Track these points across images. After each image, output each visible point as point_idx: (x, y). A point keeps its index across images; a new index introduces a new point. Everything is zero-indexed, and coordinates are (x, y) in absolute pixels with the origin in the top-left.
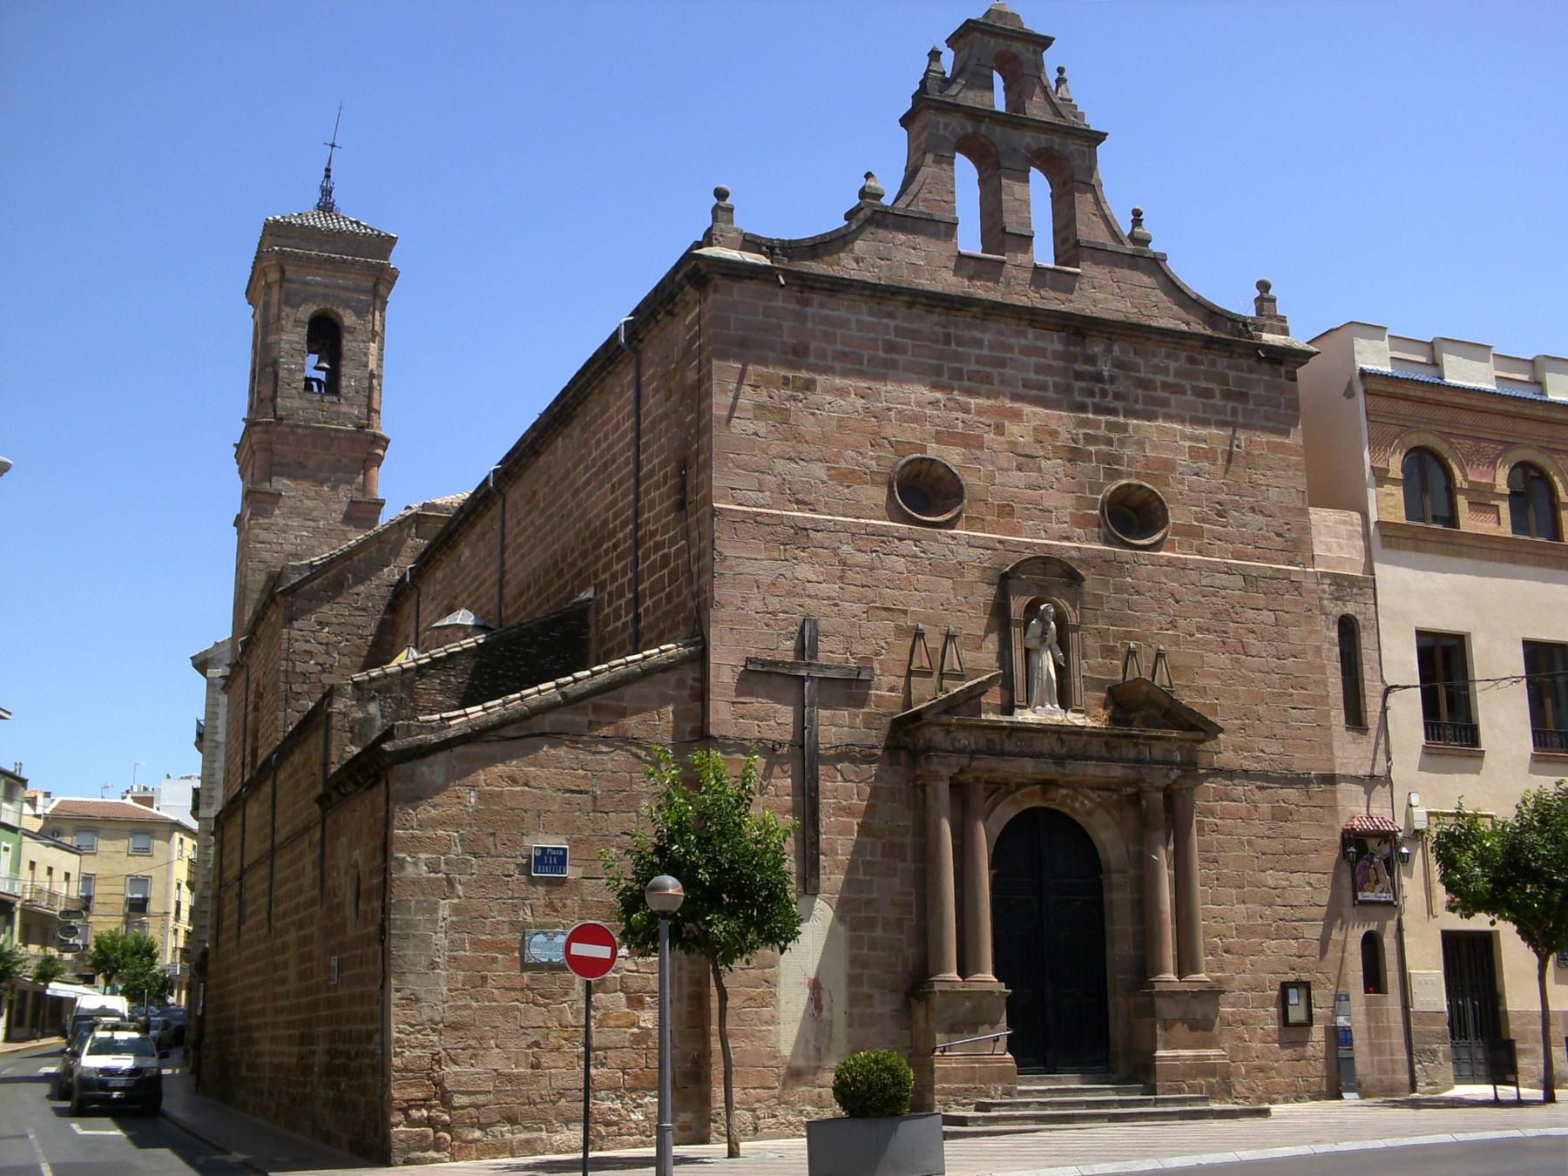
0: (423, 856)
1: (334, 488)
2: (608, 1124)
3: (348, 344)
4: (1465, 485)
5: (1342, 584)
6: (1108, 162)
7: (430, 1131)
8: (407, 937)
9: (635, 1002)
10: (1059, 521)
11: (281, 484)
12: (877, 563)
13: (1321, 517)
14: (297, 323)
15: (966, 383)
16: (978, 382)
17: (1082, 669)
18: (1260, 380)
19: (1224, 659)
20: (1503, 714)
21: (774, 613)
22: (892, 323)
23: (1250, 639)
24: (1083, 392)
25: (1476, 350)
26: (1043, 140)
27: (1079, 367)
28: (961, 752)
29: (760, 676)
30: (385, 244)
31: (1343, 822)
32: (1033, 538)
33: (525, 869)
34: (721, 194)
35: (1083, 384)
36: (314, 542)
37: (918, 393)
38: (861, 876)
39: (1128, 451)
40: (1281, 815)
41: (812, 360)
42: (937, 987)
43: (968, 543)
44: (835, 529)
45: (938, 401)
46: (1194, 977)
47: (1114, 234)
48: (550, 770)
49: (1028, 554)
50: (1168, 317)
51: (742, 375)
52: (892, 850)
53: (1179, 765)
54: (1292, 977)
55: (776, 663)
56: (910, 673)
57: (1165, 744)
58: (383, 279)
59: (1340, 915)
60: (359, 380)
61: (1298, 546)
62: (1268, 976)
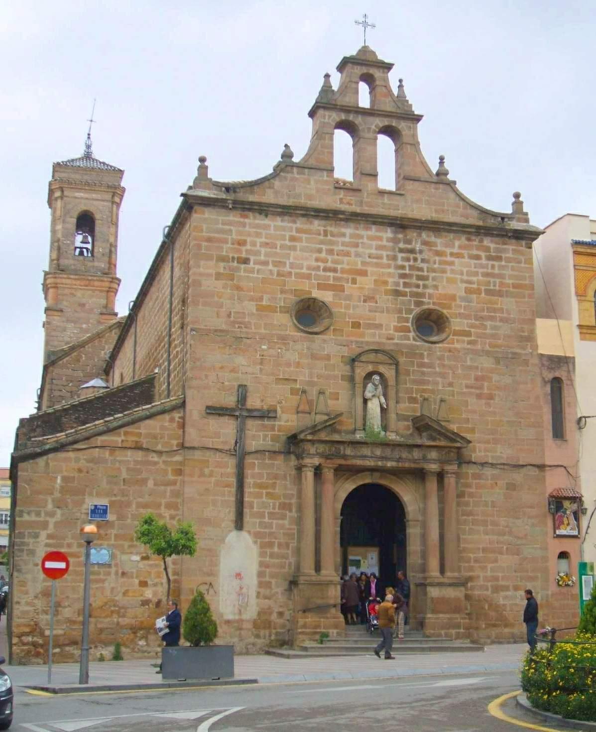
3: (98, 228)
15: (336, 257)
27: (402, 245)
32: (371, 337)
35: (403, 255)
38: (266, 520)
43: (332, 346)
47: (429, 171)
58: (116, 193)
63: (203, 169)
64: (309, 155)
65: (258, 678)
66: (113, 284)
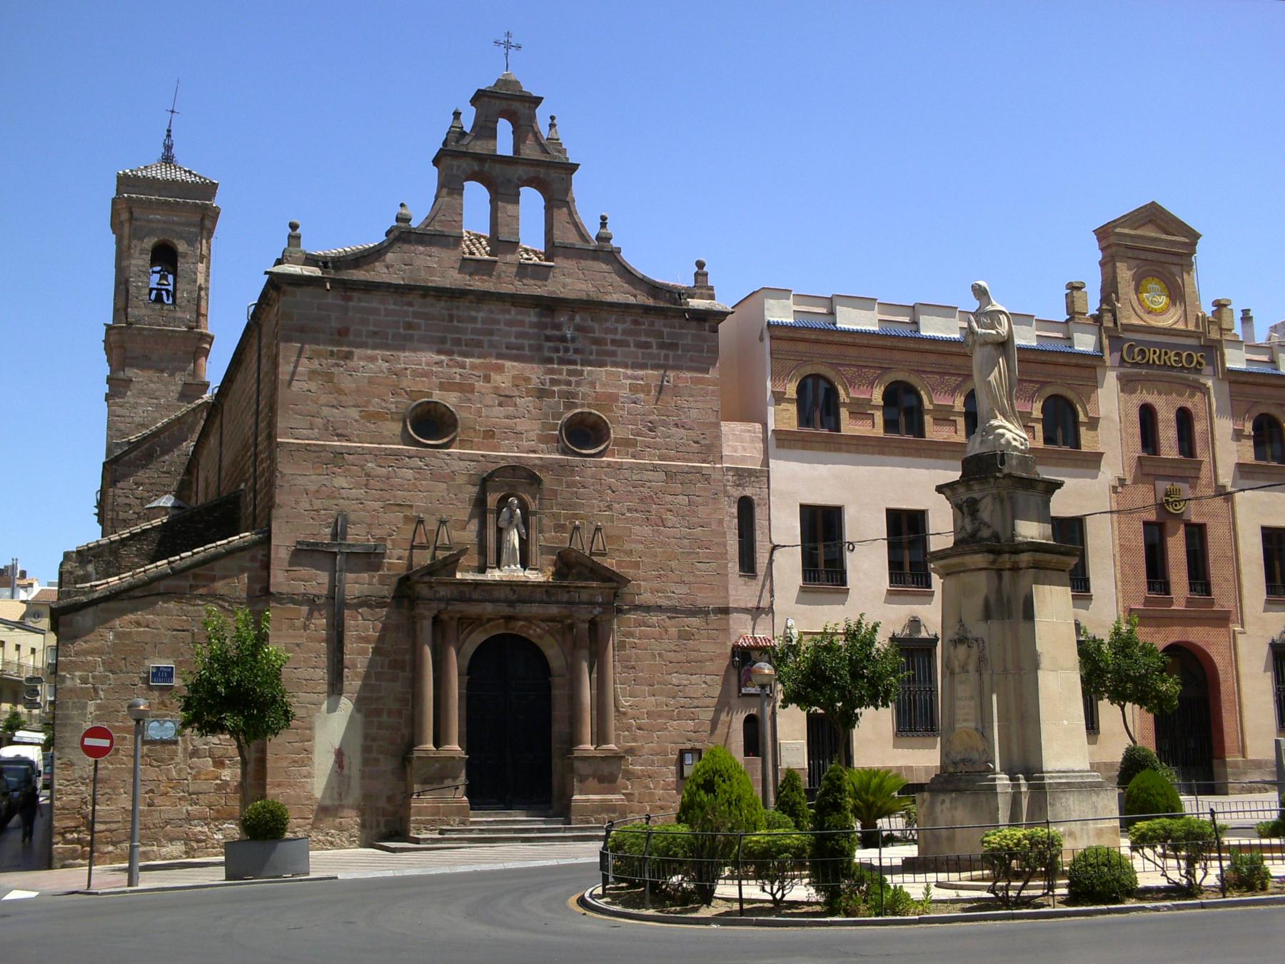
0: (77, 673)
1: (172, 375)
2: (199, 841)
3: (182, 265)
4: (847, 401)
5: (742, 475)
6: (580, 186)
7: (79, 847)
8: (65, 725)
9: (219, 763)
10: (528, 440)
11: (130, 372)
12: (392, 474)
13: (730, 429)
14: (142, 251)
15: (464, 348)
16: (471, 347)
17: (539, 540)
18: (689, 334)
19: (647, 530)
20: (868, 564)
21: (317, 511)
22: (411, 309)
23: (669, 516)
24: (550, 349)
25: (865, 303)
26: (531, 172)
27: (549, 332)
28: (440, 600)
29: (305, 553)
30: (209, 189)
31: (733, 639)
32: (508, 453)
33: (146, 680)
34: (294, 226)
35: (551, 344)
36: (157, 415)
37: (426, 358)
39: (583, 389)
40: (684, 636)
41: (351, 338)
42: (416, 754)
43: (461, 458)
44: (363, 452)
45: (442, 361)
46: (604, 747)
47: (583, 236)
48: (163, 618)
49: (503, 463)
50: (620, 294)
51: (301, 351)
52: (396, 665)
53: (600, 605)
54: (688, 746)
55: (317, 544)
56: (413, 547)
57: (591, 592)
58: (206, 220)
59: (728, 704)
60: (190, 292)
61: (711, 449)
62: (670, 746)
63: (294, 239)
64: (431, 219)
65: (877, 620)
66: (198, 344)
